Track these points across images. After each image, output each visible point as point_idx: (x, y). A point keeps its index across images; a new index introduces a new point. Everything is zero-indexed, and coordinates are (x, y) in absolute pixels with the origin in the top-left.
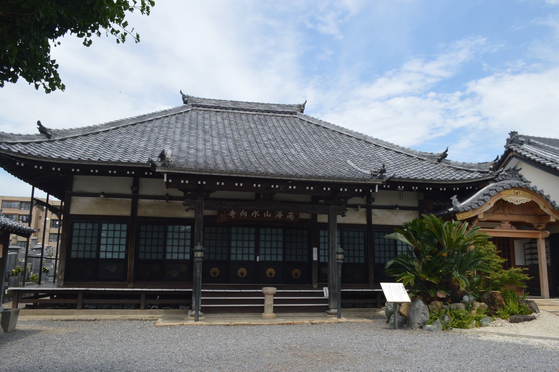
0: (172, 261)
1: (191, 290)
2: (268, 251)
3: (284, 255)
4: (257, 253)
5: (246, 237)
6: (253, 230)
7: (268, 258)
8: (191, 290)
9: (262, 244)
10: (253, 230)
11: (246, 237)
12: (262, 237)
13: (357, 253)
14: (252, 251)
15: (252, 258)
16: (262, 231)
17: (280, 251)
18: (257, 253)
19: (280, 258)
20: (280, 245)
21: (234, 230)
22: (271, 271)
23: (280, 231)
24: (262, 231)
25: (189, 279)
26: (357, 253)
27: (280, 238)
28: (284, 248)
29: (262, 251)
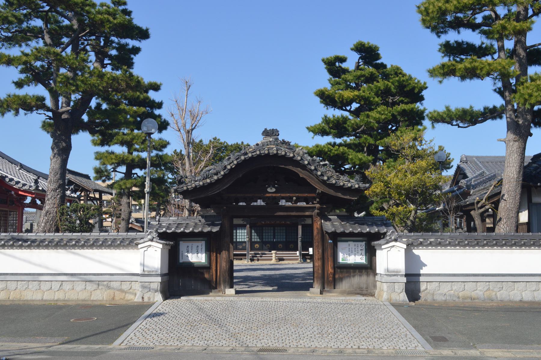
0: (239, 242)
1: (300, 228)
2: (279, 237)
3: (286, 238)
4: (274, 238)
5: (282, 234)
6: (272, 228)
7: (279, 240)
8: (300, 228)
9: (276, 234)
10: (272, 228)
11: (282, 234)
12: (276, 231)
13: (240, 234)
14: (272, 237)
15: (272, 240)
16: (276, 228)
17: (284, 237)
18: (274, 238)
19: (284, 240)
20: (284, 234)
21: (264, 228)
22: (280, 245)
23: (284, 228)
24: (276, 228)
25: (244, 249)
26: (240, 234)
27: (284, 231)
28: (286, 236)
29: (276, 237)
